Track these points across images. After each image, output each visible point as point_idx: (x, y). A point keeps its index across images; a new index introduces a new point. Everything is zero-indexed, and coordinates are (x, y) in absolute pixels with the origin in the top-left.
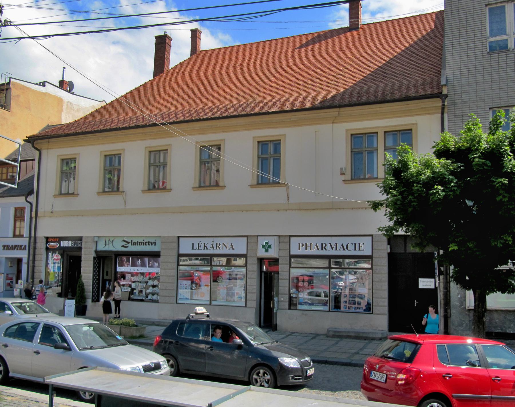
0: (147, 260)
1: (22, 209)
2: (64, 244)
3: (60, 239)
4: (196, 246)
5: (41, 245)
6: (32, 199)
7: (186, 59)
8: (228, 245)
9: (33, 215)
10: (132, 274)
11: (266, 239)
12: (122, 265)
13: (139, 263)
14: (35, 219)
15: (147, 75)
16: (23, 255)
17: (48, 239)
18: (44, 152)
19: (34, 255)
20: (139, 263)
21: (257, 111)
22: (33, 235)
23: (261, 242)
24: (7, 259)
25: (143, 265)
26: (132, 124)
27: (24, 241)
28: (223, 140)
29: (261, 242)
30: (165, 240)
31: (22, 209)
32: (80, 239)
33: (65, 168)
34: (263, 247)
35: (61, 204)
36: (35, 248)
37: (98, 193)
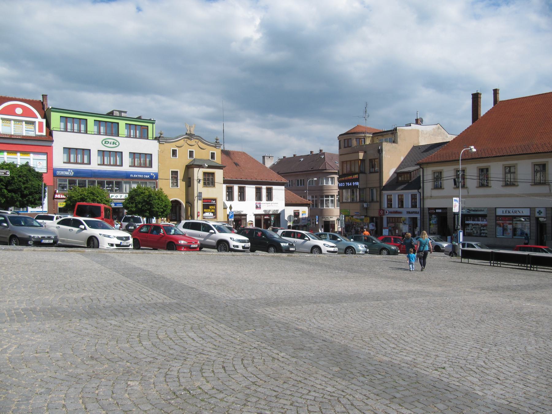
0: (480, 218)
1: (415, 195)
2: (437, 211)
3: (436, 209)
4: (504, 212)
5: (426, 212)
6: (421, 191)
7: (491, 108)
8: (521, 212)
9: (422, 197)
10: (472, 225)
11: (540, 209)
12: (468, 220)
13: (476, 219)
14: (423, 199)
15: (468, 122)
16: (418, 216)
17: (429, 209)
18: (425, 169)
19: (423, 216)
20: (476, 219)
21: (534, 151)
22: (422, 206)
23: (537, 210)
24: (409, 218)
25: (478, 220)
26: (470, 157)
27: (417, 210)
28: (517, 164)
29: (537, 210)
30: (489, 209)
31: (415, 195)
32: (446, 208)
33: (371, 170)
34: (538, 212)
35: (436, 193)
36: (423, 213)
37: (477, 187)
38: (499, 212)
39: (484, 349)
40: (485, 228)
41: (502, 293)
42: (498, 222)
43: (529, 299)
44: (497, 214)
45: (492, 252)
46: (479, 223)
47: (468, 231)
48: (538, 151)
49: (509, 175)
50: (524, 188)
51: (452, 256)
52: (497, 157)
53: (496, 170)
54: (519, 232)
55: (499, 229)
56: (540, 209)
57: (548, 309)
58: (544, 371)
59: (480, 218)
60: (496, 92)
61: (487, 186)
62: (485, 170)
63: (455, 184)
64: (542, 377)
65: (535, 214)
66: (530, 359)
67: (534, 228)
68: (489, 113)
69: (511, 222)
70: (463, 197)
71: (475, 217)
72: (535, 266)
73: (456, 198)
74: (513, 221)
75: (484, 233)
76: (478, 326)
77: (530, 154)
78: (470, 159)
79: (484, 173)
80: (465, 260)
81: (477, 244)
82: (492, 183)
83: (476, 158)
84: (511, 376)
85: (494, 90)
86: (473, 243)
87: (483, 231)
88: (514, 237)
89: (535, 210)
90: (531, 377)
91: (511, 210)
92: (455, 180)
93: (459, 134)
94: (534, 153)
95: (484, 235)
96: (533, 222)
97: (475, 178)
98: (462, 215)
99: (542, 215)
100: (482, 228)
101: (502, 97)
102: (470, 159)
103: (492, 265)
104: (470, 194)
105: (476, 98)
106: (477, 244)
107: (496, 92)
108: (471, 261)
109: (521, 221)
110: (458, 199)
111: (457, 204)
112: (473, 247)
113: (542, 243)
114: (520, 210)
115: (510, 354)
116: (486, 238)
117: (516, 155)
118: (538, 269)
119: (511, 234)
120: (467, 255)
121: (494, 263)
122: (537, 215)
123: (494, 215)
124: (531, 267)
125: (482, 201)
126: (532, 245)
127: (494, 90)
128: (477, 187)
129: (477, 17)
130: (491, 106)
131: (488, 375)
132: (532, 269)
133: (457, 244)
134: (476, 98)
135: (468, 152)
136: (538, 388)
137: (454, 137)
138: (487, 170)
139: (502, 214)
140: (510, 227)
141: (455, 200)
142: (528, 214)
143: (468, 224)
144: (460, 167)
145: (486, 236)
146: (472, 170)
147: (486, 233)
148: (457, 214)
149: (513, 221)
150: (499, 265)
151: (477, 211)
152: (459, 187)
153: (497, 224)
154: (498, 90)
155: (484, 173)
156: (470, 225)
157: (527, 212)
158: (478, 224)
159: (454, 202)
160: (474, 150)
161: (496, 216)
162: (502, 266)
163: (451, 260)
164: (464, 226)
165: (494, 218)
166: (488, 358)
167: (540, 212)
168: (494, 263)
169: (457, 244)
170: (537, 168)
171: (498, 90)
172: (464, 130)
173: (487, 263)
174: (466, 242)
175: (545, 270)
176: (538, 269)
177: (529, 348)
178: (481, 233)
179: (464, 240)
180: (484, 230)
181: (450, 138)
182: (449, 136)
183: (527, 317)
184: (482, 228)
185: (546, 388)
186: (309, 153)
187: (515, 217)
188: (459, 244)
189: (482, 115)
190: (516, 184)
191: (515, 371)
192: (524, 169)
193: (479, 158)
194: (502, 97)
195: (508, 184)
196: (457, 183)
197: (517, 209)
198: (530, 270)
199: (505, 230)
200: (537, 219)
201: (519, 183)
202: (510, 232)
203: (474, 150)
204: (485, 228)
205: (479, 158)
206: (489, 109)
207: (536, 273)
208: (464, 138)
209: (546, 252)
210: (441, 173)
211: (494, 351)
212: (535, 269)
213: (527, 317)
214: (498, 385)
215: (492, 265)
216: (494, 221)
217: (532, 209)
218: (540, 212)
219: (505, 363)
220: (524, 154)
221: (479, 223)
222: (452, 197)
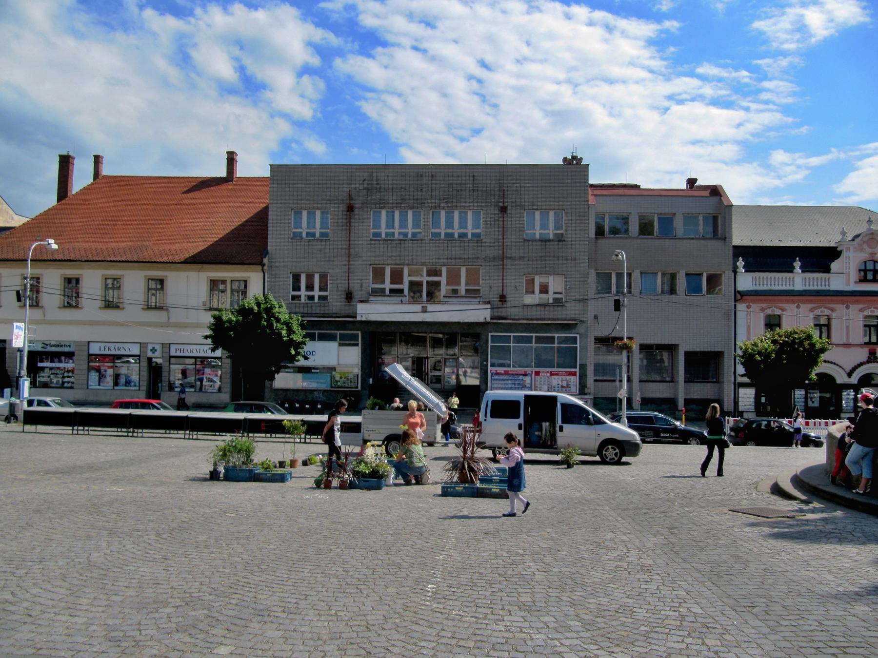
4: (102, 349)
10: (51, 369)
11: (154, 345)
12: (42, 361)
13: (56, 360)
15: (51, 200)
23: (150, 347)
25: (60, 361)
26: (50, 258)
28: (123, 276)
29: (150, 347)
30: (78, 344)
37: (59, 308)
38: (95, 349)
39: (18, 572)
40: (70, 374)
41: (79, 476)
42: (91, 364)
43: (116, 481)
44: (91, 352)
45: (76, 413)
46: (61, 365)
47: (42, 379)
48: (154, 259)
49: (111, 291)
50: (133, 312)
51: (9, 422)
52: (93, 261)
53: (92, 282)
54: (122, 380)
55: (94, 375)
56: (154, 345)
57: (140, 491)
58: (107, 587)
59: (63, 358)
60: (97, 160)
61: (76, 307)
62: (74, 282)
63: (19, 300)
64: (101, 596)
65: (146, 352)
66: (92, 572)
67: (145, 374)
68: (85, 190)
69: (111, 364)
70: (31, 322)
71: (54, 356)
72: (140, 431)
73: (18, 324)
74: (114, 362)
75: (68, 382)
76: (21, 535)
77: (143, 262)
78: (45, 260)
79: (72, 284)
80: (28, 428)
81: (54, 401)
82: (84, 302)
83: (59, 261)
84: (53, 606)
85: (95, 156)
86: (48, 399)
87: (66, 380)
88: (116, 388)
89: (147, 347)
90: (85, 600)
91: (112, 346)
92: (18, 293)
93: (33, 216)
94: (149, 262)
95: (70, 385)
96: (144, 364)
97: (58, 292)
98: (29, 352)
99: (157, 354)
100: (66, 374)
101: (106, 170)
102: (45, 260)
103: (75, 432)
104: (47, 318)
105: (65, 163)
106: (54, 401)
107: (97, 160)
108: (41, 428)
109: (128, 362)
110: (22, 325)
111: (22, 333)
112: (47, 404)
113: (157, 397)
114: (126, 346)
115: (61, 571)
116: (71, 390)
117: (122, 262)
118: (144, 435)
119: (111, 384)
120: (32, 418)
121: (78, 430)
122: (150, 354)
123: (86, 353)
124: (133, 432)
125: (67, 329)
126: (142, 398)
127: (95, 156)
128: (59, 308)
129: (76, 34)
130: (90, 180)
131: (13, 613)
132: (135, 435)
133: (18, 401)
134: (65, 163)
135: (46, 249)
136: (90, 615)
137: (25, 220)
138: (77, 281)
139: (98, 352)
140: (110, 372)
141: (18, 327)
142: (138, 353)
143: (43, 369)
144: (29, 271)
145: (72, 388)
146: (52, 280)
147: (73, 383)
148: (20, 350)
149: (114, 362)
150: (86, 432)
151: (62, 346)
152: (25, 305)
153: (90, 369)
154: (102, 158)
155: (72, 284)
156: (47, 370)
157: (135, 350)
158: (59, 368)
159: (15, 331)
160: (55, 247)
161: (90, 355)
162: (91, 433)
163: (5, 429)
164: (33, 370)
165: (86, 358)
166: (22, 584)
167: (154, 350)
168: (78, 430)
169: (18, 401)
170: (153, 285)
171: (102, 158)
172: (42, 211)
173: (68, 429)
174: (36, 398)
175: (288, 440)
176: (144, 435)
177: (95, 555)
178: (63, 383)
179: (30, 394)
180: (68, 377)
181: (17, 221)
182: (16, 217)
183: (105, 509)
184: (66, 374)
185: (103, 612)
186: (683, 186)
187: (119, 357)
188: (22, 401)
189: (74, 192)
190: (121, 306)
191: (61, 597)
192: (134, 283)
193: (65, 261)
194: (106, 170)
195: (110, 305)
196: (23, 299)
197: (121, 345)
198: (305, 443)
199: (102, 377)
200: (150, 360)
201: (125, 306)
202: (109, 380)
203: (55, 247)
204: (70, 374)
205: (65, 261)
206: (85, 185)
207: (139, 440)
208: (40, 225)
209: (158, 409)
210: (38, 278)
211: (37, 571)
212: (140, 435)
213: (105, 509)
214: (27, 626)
215: (75, 432)
216: (86, 362)
217: (143, 345)
218: (154, 350)
219: (49, 587)
220: (134, 262)
221: (61, 365)
222: (10, 322)
